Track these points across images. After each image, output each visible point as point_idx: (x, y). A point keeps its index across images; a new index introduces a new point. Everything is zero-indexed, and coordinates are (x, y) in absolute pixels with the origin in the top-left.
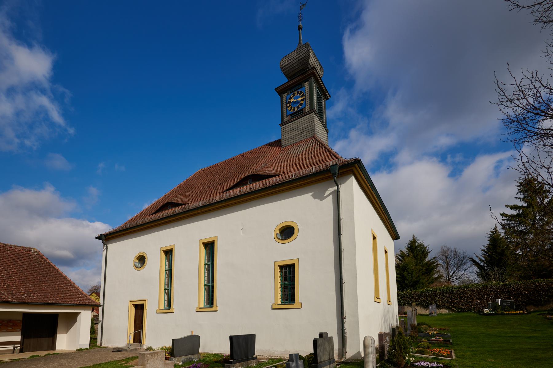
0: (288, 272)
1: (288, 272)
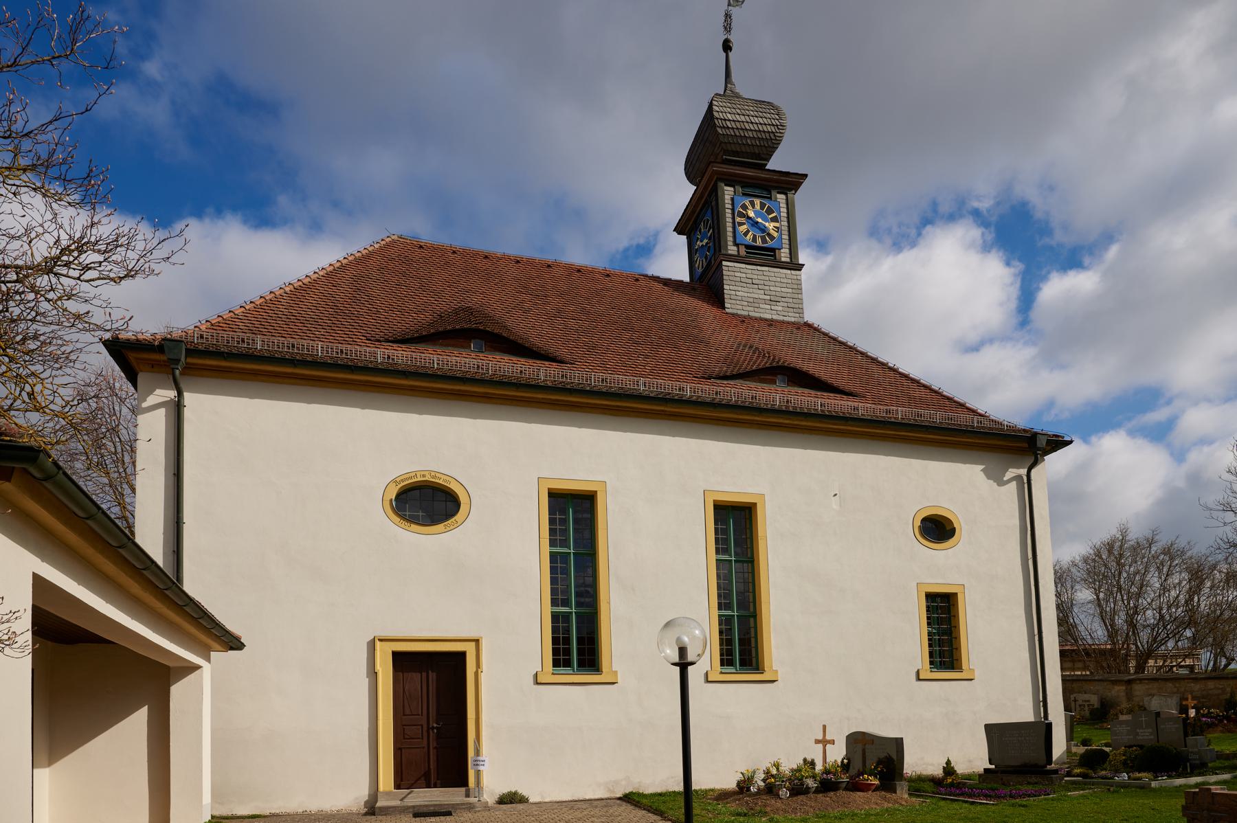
0: (942, 611)
1: (942, 611)
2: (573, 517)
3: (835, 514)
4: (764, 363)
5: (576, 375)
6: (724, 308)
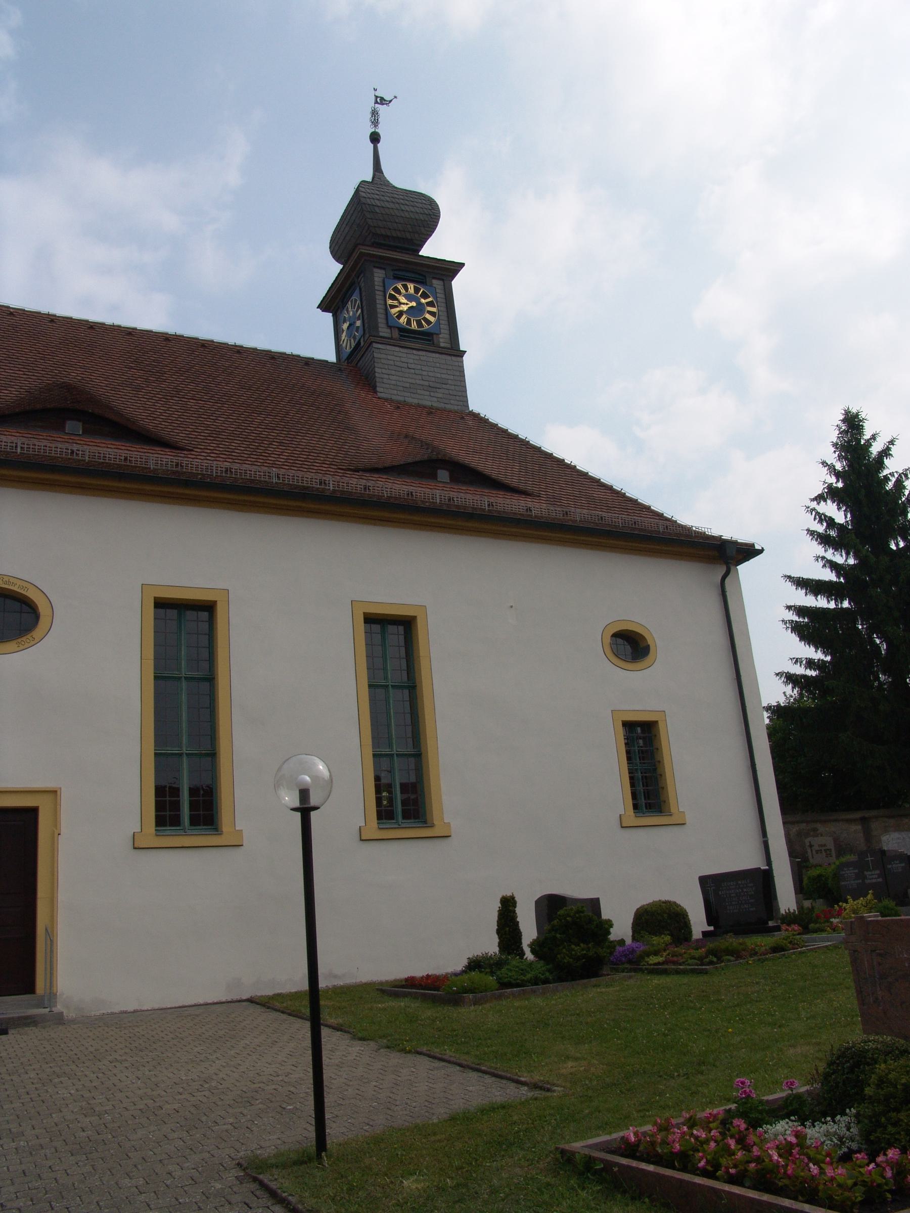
0: (642, 742)
1: (642, 742)
2: (186, 632)
3: (502, 629)
4: (420, 455)
5: (195, 463)
6: (375, 392)
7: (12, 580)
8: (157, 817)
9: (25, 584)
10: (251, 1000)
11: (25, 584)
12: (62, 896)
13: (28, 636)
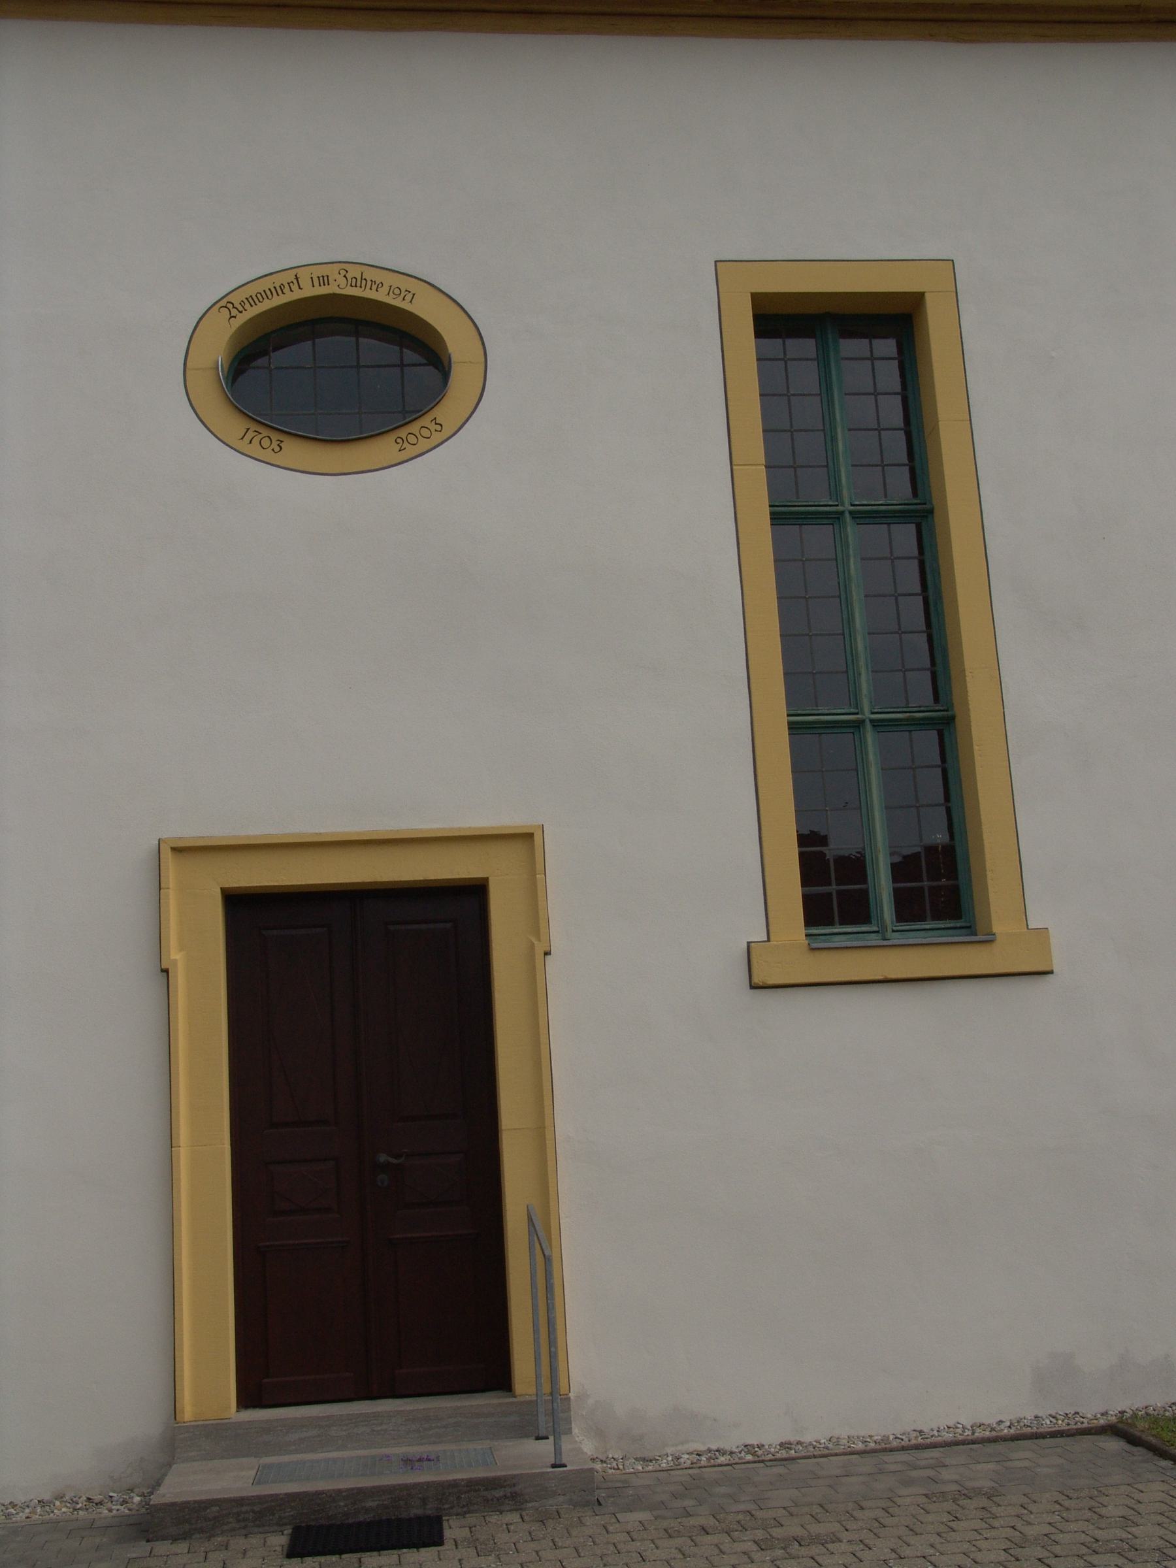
7: (370, 274)
8: (807, 900)
9: (405, 283)
10: (1120, 1430)
11: (405, 283)
12: (566, 1124)
13: (426, 421)
